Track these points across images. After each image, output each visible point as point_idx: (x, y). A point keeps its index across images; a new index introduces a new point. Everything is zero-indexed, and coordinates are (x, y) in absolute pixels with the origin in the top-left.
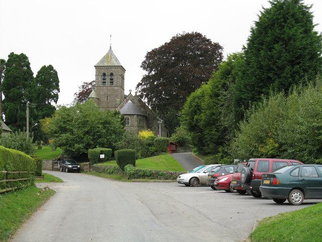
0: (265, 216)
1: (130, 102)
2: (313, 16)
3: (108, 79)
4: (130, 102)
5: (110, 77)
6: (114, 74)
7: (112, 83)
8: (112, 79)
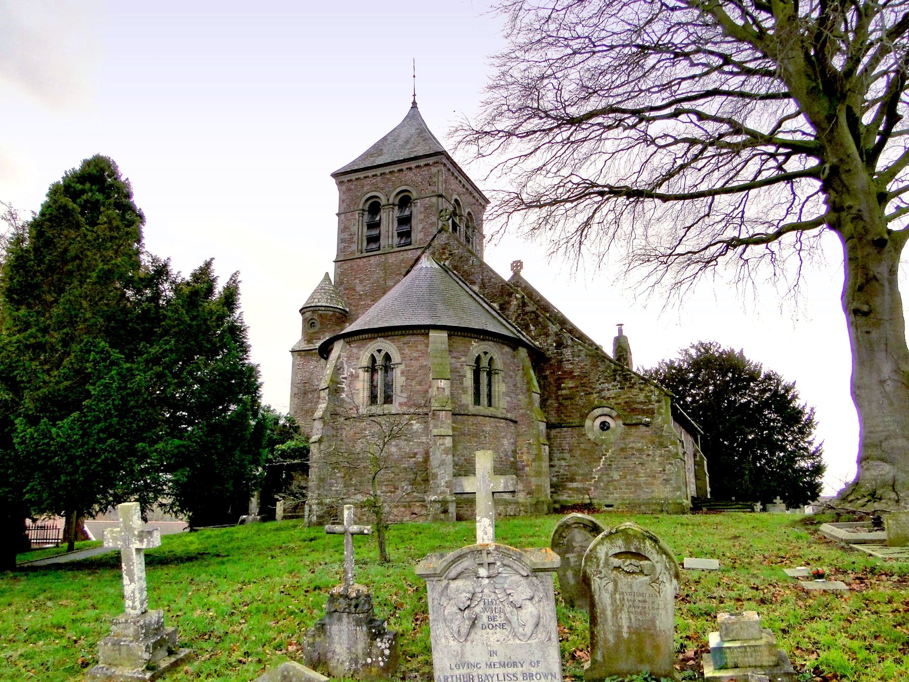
0: (742, 514)
1: (426, 263)
2: (230, 298)
3: (388, 220)
4: (426, 263)
5: (396, 213)
6: (414, 195)
7: (405, 235)
8: (405, 221)
